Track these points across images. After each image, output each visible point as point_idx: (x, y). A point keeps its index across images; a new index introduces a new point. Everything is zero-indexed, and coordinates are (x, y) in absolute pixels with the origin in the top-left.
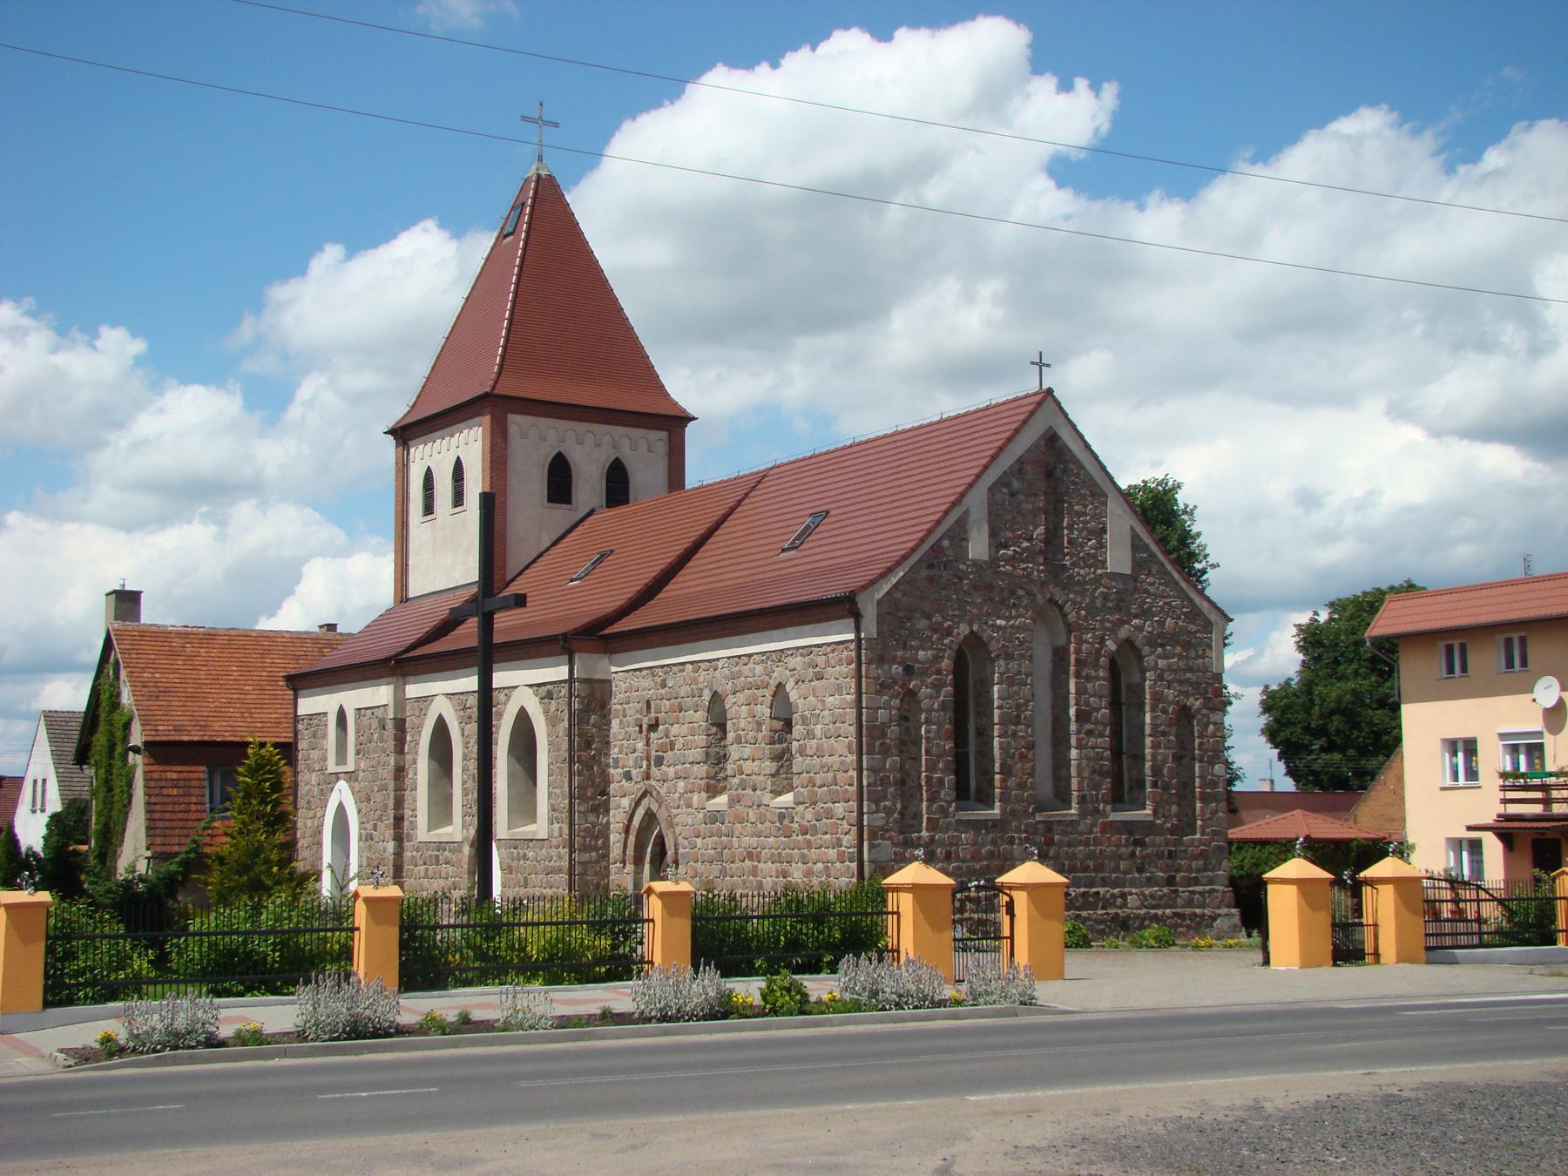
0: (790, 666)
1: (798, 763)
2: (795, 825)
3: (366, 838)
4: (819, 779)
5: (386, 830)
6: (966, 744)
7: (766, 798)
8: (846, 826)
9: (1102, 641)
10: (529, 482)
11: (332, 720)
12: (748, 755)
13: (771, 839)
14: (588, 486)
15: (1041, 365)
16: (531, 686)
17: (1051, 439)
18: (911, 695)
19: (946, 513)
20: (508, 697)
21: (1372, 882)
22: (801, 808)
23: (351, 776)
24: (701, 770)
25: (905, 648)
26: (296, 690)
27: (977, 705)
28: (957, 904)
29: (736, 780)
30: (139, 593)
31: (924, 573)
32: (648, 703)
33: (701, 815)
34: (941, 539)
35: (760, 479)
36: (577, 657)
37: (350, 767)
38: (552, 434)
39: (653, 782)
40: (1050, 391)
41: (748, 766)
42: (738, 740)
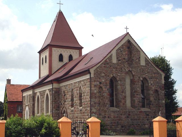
9: (139, 78)
10: (55, 57)
11: (26, 97)
12: (76, 100)
14: (66, 59)
15: (127, 28)
16: (48, 89)
17: (129, 41)
19: (108, 55)
21: (178, 121)
22: (83, 109)
23: (28, 105)
24: (70, 103)
25: (100, 79)
27: (115, 90)
28: (73, 128)
29: (75, 104)
30: (11, 80)
31: (103, 65)
33: (70, 111)
34: (107, 59)
35: (88, 54)
36: (54, 84)
37: (28, 104)
38: (60, 51)
40: (128, 33)
41: (76, 102)
42: (75, 97)
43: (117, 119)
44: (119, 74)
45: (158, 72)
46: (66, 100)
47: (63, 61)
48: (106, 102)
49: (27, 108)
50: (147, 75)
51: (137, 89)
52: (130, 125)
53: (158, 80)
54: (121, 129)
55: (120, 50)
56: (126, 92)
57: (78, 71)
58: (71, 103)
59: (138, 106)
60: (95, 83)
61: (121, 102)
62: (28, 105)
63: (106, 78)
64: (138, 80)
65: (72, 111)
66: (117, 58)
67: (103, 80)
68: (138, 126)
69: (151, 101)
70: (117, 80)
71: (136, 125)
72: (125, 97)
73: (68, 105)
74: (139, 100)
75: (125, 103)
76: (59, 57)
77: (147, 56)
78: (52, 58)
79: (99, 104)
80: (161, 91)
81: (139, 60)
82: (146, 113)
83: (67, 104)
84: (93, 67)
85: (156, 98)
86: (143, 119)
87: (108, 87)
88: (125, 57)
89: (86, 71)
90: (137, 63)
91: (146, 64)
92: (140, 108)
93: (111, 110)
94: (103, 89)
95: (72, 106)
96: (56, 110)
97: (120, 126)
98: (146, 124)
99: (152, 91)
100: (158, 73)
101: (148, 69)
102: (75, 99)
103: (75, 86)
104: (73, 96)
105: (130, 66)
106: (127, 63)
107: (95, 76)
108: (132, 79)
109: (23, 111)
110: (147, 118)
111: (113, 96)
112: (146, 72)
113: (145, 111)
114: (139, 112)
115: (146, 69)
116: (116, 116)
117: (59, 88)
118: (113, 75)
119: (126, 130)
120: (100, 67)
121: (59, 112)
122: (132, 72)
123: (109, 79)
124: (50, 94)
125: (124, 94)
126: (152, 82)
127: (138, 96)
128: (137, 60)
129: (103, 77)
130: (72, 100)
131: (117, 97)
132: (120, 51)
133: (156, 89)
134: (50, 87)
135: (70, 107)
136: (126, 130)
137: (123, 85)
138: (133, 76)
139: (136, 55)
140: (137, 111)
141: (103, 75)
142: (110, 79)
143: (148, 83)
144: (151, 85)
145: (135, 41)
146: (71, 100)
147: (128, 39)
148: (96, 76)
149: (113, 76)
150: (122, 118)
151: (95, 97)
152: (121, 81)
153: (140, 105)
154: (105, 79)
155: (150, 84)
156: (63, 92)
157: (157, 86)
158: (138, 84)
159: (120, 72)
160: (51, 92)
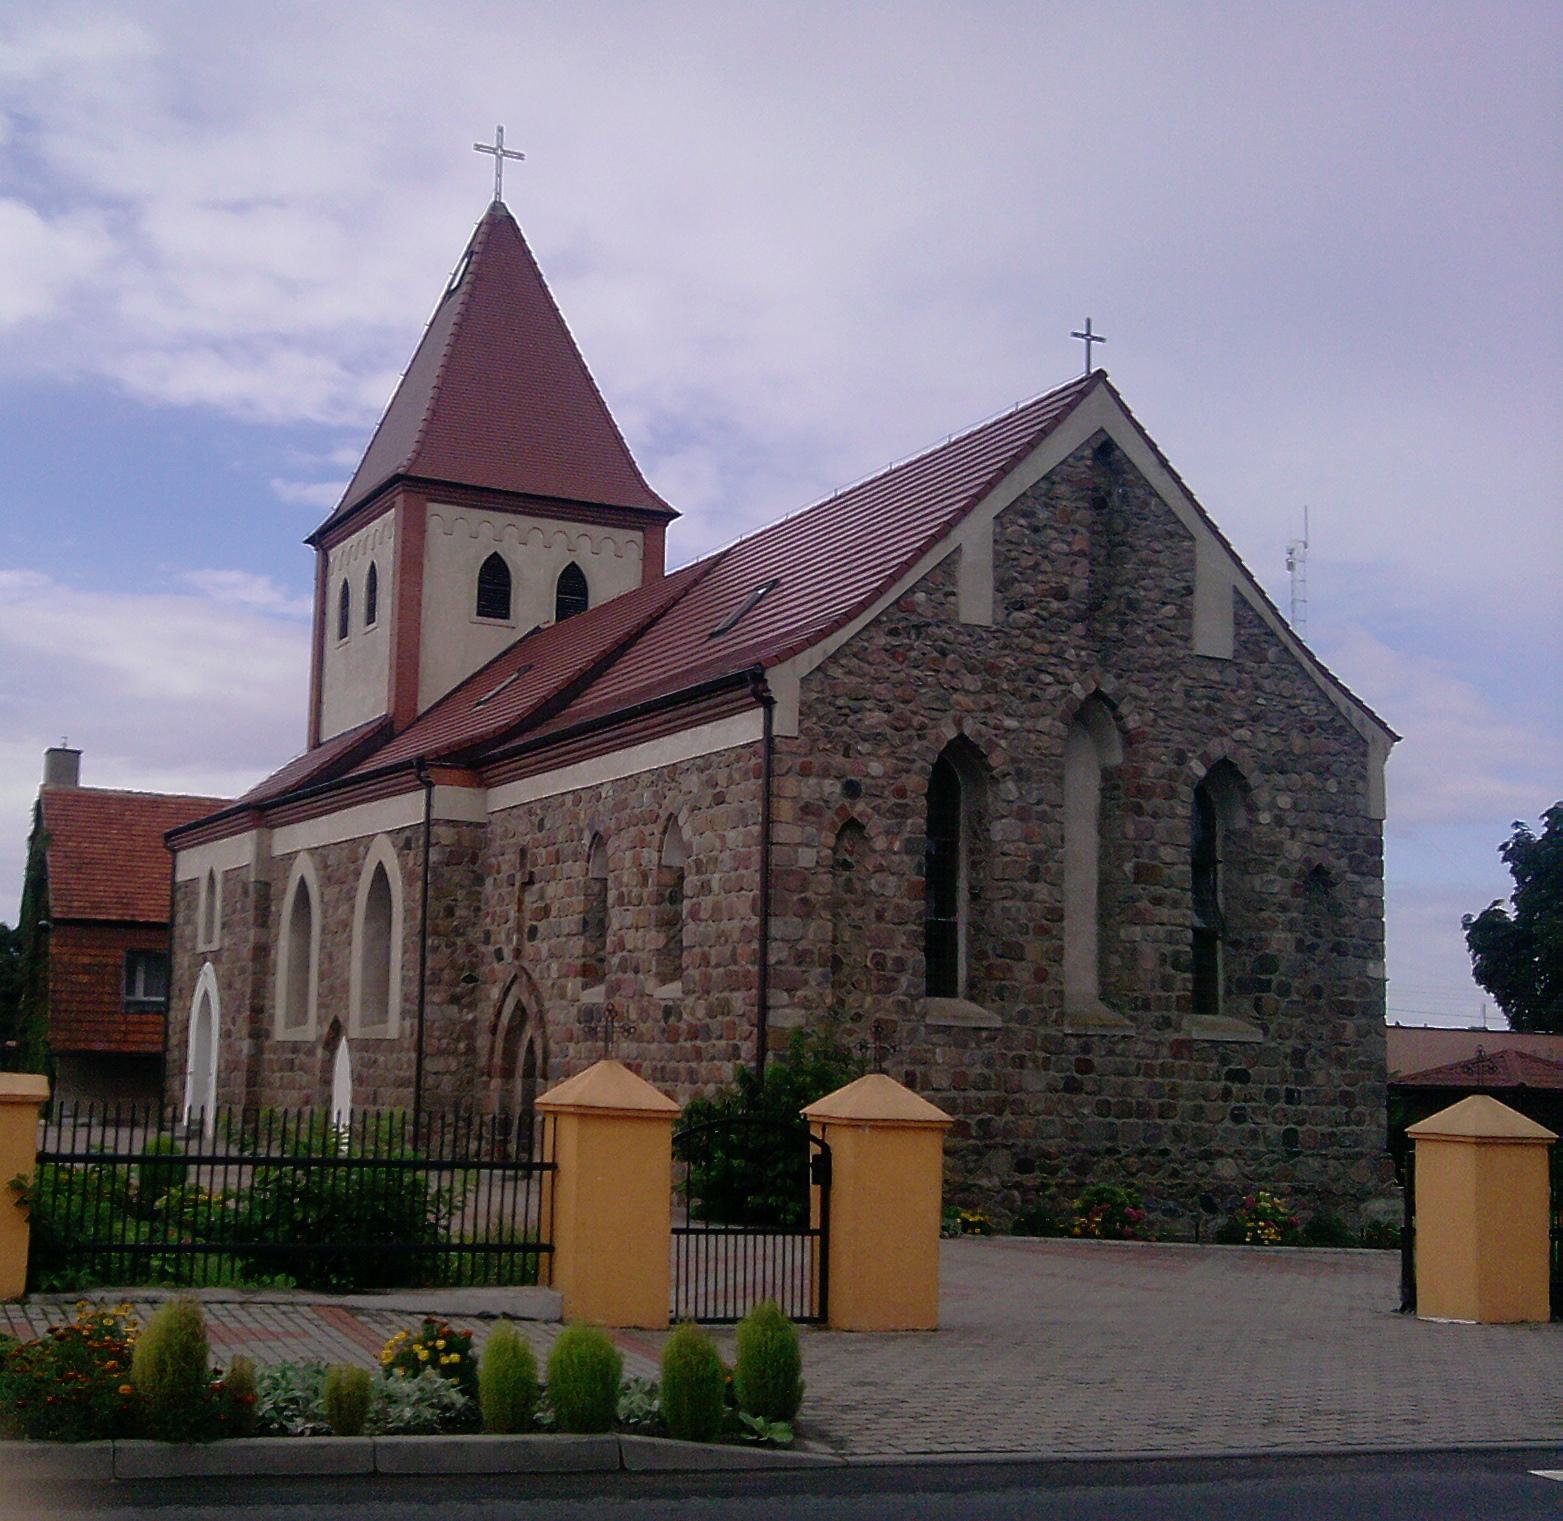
0: (684, 788)
1: (690, 933)
2: (683, 1026)
3: (226, 1034)
4: (713, 955)
5: (242, 1027)
6: (952, 910)
7: (651, 985)
8: (746, 1027)
9: (1181, 758)
10: (452, 585)
12: (633, 930)
13: (654, 1046)
17: (1104, 449)
18: (852, 827)
19: (922, 552)
20: (367, 849)
22: (690, 1000)
23: (216, 957)
24: (576, 945)
25: (846, 755)
26: (174, 852)
31: (882, 640)
32: (523, 852)
33: (574, 1010)
34: (912, 590)
37: (215, 946)
39: (526, 964)
40: (1101, 374)
41: (632, 939)
43: (982, 1095)
44: (1009, 723)
45: (1339, 723)
46: (541, 925)
47: (506, 616)
48: (892, 954)
49: (208, 980)
50: (1241, 742)
51: (1154, 855)
52: (1095, 1153)
53: (1332, 786)
54: (1017, 1186)
55: (1024, 515)
56: (1061, 873)
57: (649, 689)
58: (578, 952)
59: (1356, 947)
60: (809, 789)
61: (1015, 952)
62: (216, 957)
63: (902, 751)
64: (1171, 776)
65: (588, 1015)
66: (1002, 585)
67: (875, 768)
68: (1160, 1166)
69: (1267, 964)
70: (990, 768)
71: (1142, 1153)
72: (1056, 915)
73: (554, 966)
74: (1168, 949)
75: (1053, 970)
76: (481, 581)
77: (1249, 577)
78: (420, 584)
79: (836, 963)
80: (1356, 878)
81: (1185, 614)
82: (1224, 1061)
83: (544, 952)
84: (794, 651)
85: (1318, 935)
86: (1198, 1113)
87: (916, 823)
88: (1066, 580)
89: (737, 681)
90: (1166, 635)
91: (1244, 646)
92: (1174, 1015)
93: (928, 1021)
94: (867, 839)
95: (591, 972)
96: (455, 1000)
97: (1001, 1161)
98: (1220, 1154)
99: (1284, 873)
100: (1341, 731)
101: (1258, 687)
102: (617, 918)
103: (620, 806)
104: (605, 889)
105: (1105, 658)
106: (1079, 628)
107: (807, 724)
108: (1118, 769)
109: (175, 1003)
110: (1233, 1104)
111: (954, 901)
112: (1238, 716)
113: (1215, 1044)
114: (1165, 1051)
115: (1241, 692)
116: (978, 1069)
117: (482, 825)
118: (958, 723)
119: (1053, 1190)
120: (855, 655)
121: (470, 1017)
122: (1124, 709)
123: (923, 754)
124: (403, 867)
125: (1042, 891)
126: (1284, 801)
127: (1164, 913)
128: (1169, 610)
129: (877, 738)
130: (595, 924)
131: (982, 913)
132: (1022, 521)
133: (1317, 857)
134: (405, 809)
135: (572, 985)
136: (1053, 1190)
137: (1043, 817)
138: (1130, 739)
139: (1156, 564)
140: (1153, 1035)
141: (875, 718)
142: (933, 758)
143: (1252, 809)
144: (1279, 821)
145: (1153, 447)
146: (585, 922)
147: (1102, 430)
148: (817, 729)
149: (961, 736)
150: (1020, 1089)
151: (805, 901)
152: (1021, 776)
153: (1179, 985)
154: (892, 754)
155: (1265, 818)
156: (511, 857)
157: (1321, 837)
158: (1173, 816)
159: (1016, 702)
160: (414, 858)
